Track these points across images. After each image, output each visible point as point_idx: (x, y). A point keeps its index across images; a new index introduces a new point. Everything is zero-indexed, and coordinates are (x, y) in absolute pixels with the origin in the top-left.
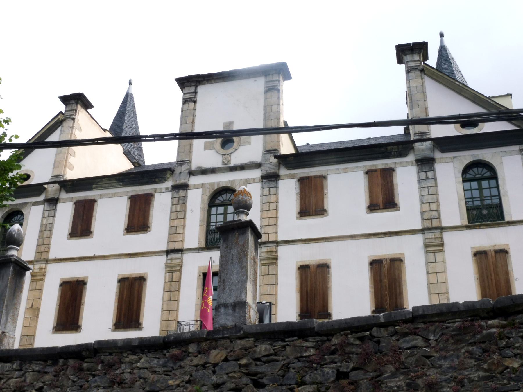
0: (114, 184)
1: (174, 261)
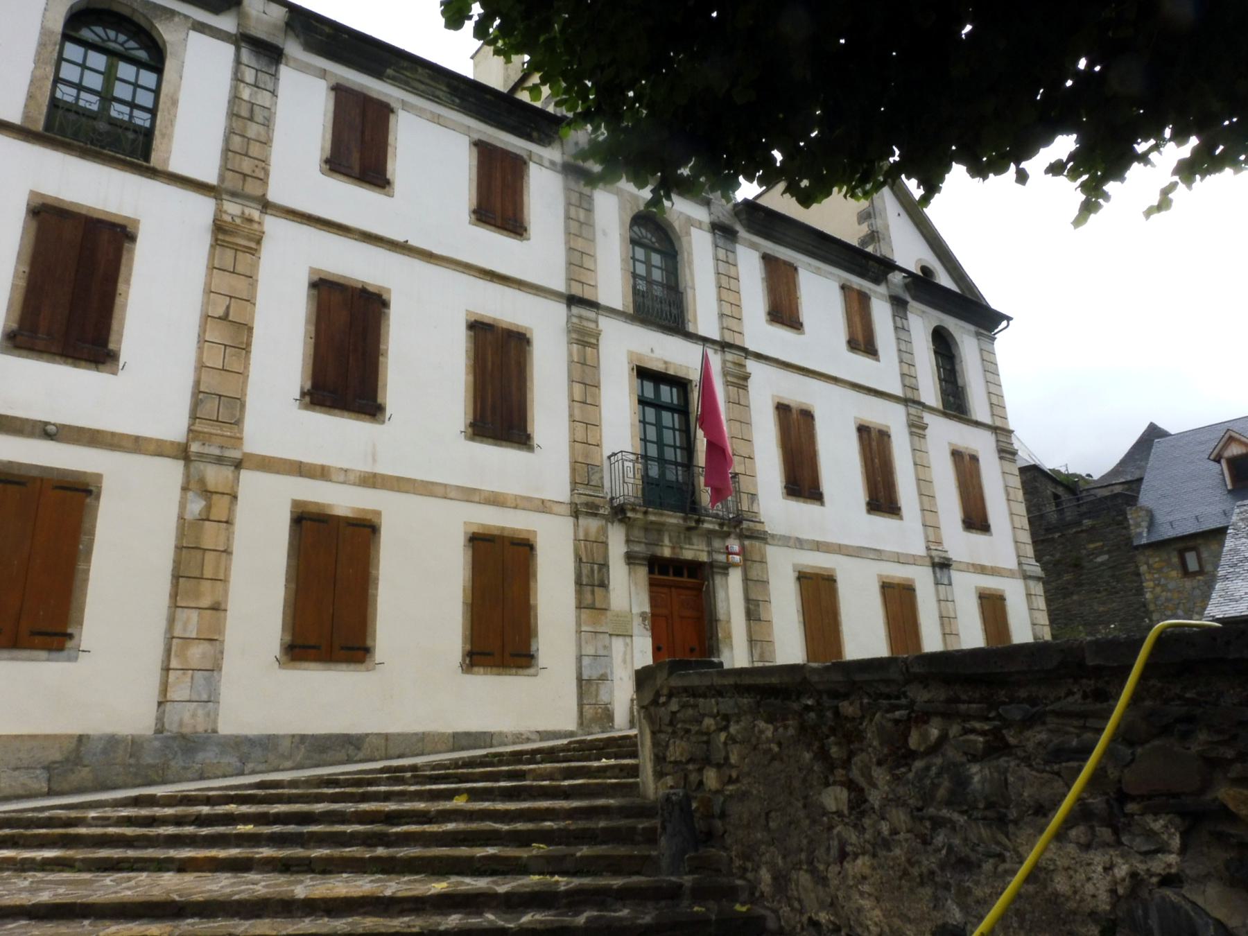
0: (440, 94)
1: (585, 323)
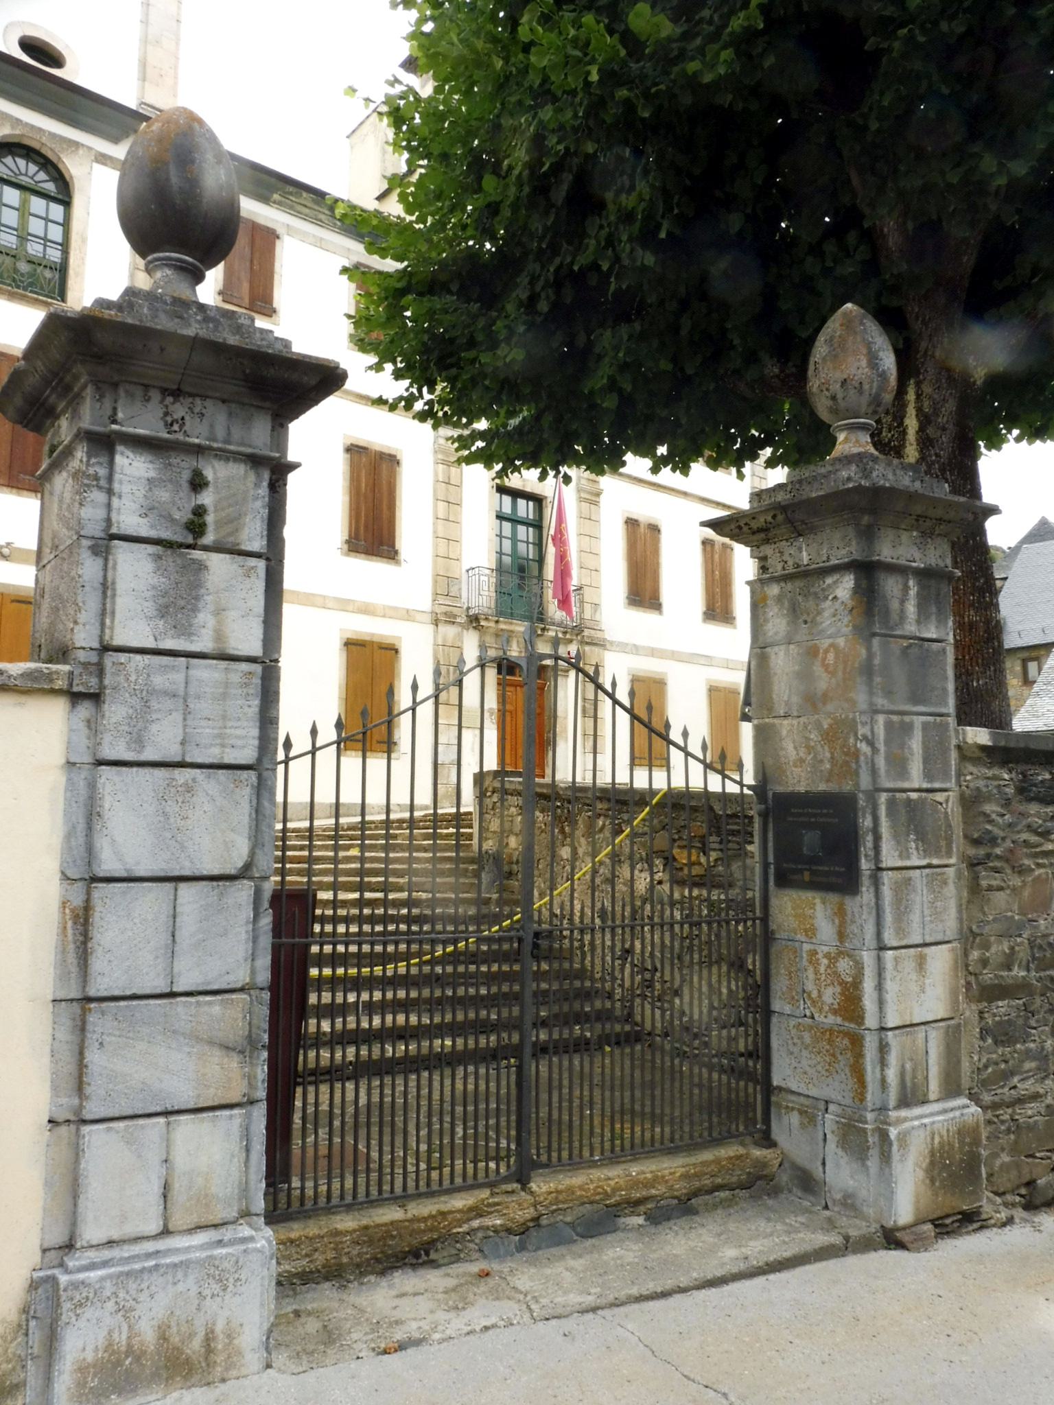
0: (322, 217)
